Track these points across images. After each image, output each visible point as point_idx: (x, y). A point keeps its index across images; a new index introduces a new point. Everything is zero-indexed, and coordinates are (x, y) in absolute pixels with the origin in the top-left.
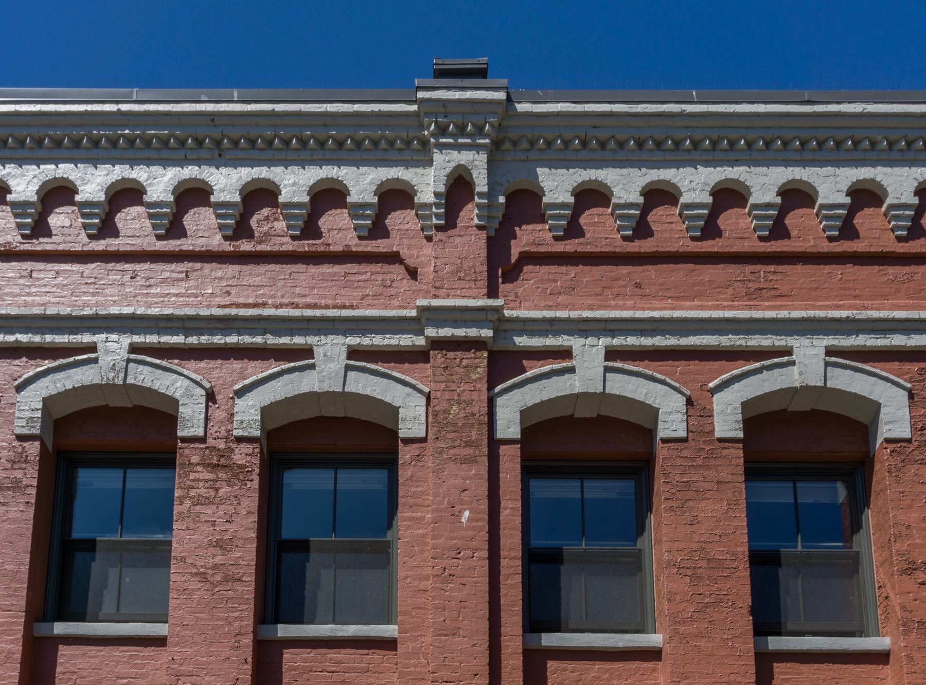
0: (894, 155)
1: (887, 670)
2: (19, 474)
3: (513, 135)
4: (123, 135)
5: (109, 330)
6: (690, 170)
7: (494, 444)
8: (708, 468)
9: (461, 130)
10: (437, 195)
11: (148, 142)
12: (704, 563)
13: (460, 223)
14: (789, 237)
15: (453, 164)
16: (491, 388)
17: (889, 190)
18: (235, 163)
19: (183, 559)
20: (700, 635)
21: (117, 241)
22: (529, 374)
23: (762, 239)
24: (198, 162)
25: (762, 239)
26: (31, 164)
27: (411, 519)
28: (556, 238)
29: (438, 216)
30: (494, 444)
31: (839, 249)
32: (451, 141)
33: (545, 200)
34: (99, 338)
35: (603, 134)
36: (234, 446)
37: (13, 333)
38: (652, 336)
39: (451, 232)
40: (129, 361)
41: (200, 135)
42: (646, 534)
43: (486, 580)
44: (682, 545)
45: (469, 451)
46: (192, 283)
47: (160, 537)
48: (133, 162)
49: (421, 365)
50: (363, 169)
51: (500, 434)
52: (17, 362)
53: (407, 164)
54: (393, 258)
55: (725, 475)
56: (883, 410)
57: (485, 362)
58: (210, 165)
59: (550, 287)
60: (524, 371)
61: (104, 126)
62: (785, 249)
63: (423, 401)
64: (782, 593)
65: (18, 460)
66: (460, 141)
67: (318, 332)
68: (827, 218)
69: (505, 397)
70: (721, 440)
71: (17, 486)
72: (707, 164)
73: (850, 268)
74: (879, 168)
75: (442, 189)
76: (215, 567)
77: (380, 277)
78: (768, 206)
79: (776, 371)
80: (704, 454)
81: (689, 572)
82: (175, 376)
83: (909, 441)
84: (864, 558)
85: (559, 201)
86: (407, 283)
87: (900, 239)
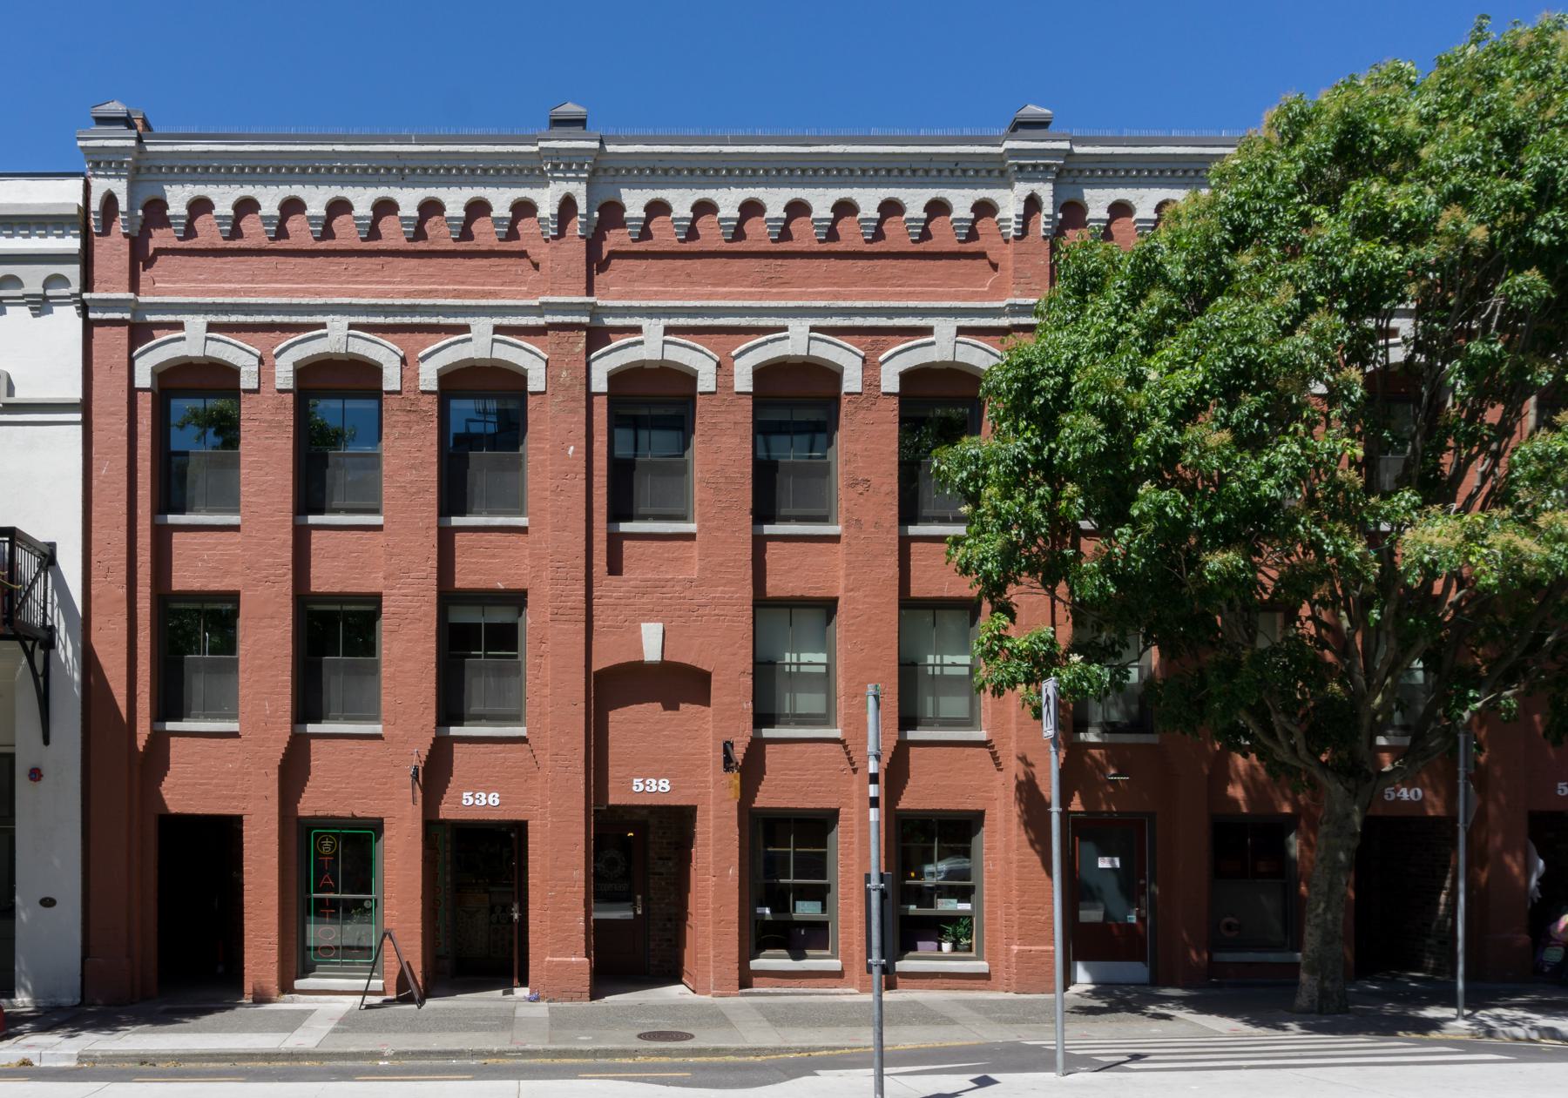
0: (866, 179)
2: (281, 418)
3: (605, 166)
4: (337, 167)
5: (334, 313)
6: (726, 190)
7: (590, 396)
8: (728, 412)
9: (568, 168)
10: (552, 215)
11: (353, 170)
12: (723, 480)
13: (568, 233)
14: (791, 239)
15: (563, 193)
16: (588, 353)
17: (861, 206)
18: (414, 185)
19: (391, 477)
20: (718, 529)
21: (334, 242)
22: (613, 345)
23: (773, 241)
24: (388, 184)
25: (773, 241)
26: (272, 185)
27: (537, 448)
28: (634, 241)
29: (553, 230)
30: (590, 396)
31: (825, 249)
32: (562, 175)
33: (626, 215)
34: (326, 319)
35: (667, 166)
36: (420, 397)
37: (270, 315)
38: (696, 318)
39: (562, 240)
40: (348, 336)
41: (389, 166)
42: (690, 449)
43: (584, 494)
44: (710, 467)
45: (573, 404)
46: (387, 273)
47: (368, 449)
48: (343, 184)
49: (542, 337)
50: (501, 189)
51: (594, 389)
52: (272, 335)
53: (532, 185)
54: (522, 254)
55: (739, 418)
56: (845, 372)
57: (584, 340)
58: (396, 186)
59: (629, 276)
61: (324, 160)
62: (788, 249)
63: (544, 365)
64: (778, 490)
65: (278, 408)
66: (568, 175)
67: (474, 315)
68: (817, 227)
69: (598, 361)
70: (738, 393)
71: (279, 424)
72: (737, 186)
73: (832, 262)
74: (855, 189)
75: (555, 211)
76: (411, 482)
77: (514, 269)
78: (777, 219)
79: (777, 343)
80: (726, 403)
81: (714, 486)
82: (379, 346)
83: (860, 394)
85: (635, 216)
86: (533, 275)
87: (867, 241)
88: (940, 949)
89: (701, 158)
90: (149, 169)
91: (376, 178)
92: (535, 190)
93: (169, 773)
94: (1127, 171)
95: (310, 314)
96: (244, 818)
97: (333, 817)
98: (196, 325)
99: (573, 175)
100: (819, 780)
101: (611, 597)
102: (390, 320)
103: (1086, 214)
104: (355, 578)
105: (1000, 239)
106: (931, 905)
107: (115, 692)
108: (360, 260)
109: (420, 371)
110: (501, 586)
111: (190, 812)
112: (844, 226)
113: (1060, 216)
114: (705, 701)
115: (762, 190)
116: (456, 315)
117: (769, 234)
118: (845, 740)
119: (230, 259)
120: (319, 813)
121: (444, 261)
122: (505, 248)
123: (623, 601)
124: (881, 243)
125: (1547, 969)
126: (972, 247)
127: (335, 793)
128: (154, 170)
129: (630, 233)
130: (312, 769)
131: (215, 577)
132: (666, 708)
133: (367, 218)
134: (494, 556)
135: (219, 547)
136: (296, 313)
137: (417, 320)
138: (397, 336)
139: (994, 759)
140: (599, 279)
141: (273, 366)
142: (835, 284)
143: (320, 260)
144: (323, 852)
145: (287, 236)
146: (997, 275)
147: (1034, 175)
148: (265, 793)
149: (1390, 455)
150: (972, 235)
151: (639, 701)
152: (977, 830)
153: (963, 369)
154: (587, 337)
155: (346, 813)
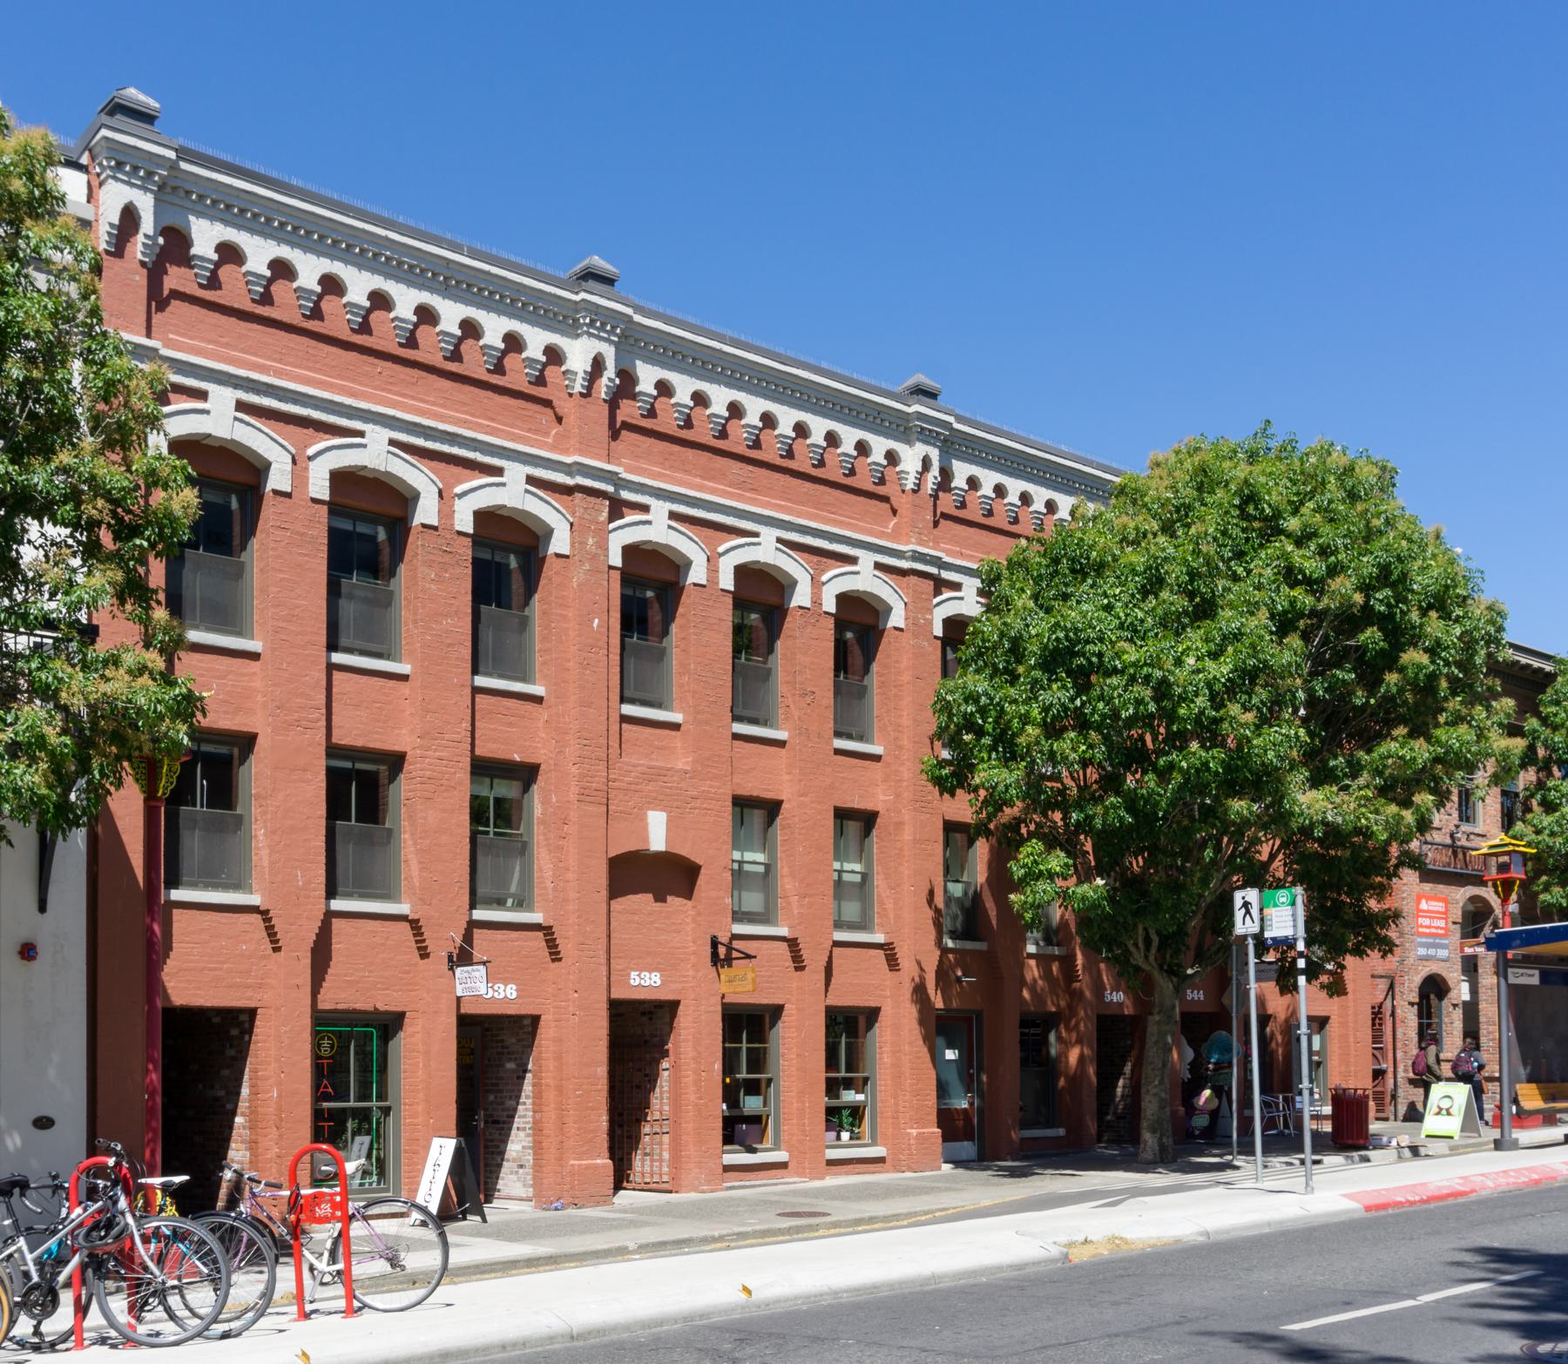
1: (783, 751)
5: (375, 422)
27: (561, 615)
28: (642, 416)
35: (676, 349)
52: (305, 431)
53: (563, 333)
54: (547, 403)
60: (622, 517)
67: (508, 458)
70: (722, 590)
84: (247, 568)
88: (838, 1138)
89: (705, 350)
90: (175, 189)
91: (420, 281)
92: (565, 339)
93: (172, 954)
94: (480, 290)
95: (350, 417)
96: (259, 1011)
97: (355, 1011)
98: (222, 399)
99: (605, 335)
100: (770, 976)
101: (622, 781)
102: (430, 445)
103: (951, 481)
104: (377, 733)
105: (898, 488)
106: (838, 1097)
107: (129, 848)
108: (394, 366)
109: (456, 508)
110: (517, 758)
111: (198, 1004)
112: (511, 361)
113: (161, 240)
114: (688, 893)
115: (744, 394)
116: (492, 454)
117: (746, 439)
118: (267, 912)
119: (255, 326)
120: (341, 1007)
121: (477, 391)
122: (534, 393)
123: (633, 787)
124: (541, 389)
125: (1197, 1133)
126: (881, 490)
127: (358, 982)
128: (182, 194)
129: (639, 408)
130: (334, 954)
131: (225, 712)
132: (657, 900)
133: (209, 261)
134: (510, 724)
135: (231, 677)
136: (333, 412)
137: (455, 451)
138: (434, 464)
139: (269, 935)
140: (157, 318)
141: (306, 469)
142: (789, 500)
143: (353, 355)
144: (323, 1053)
145: (322, 319)
146: (895, 520)
147: (929, 439)
148: (297, 981)
149: (201, 551)
150: (540, 381)
151: (635, 892)
152: (773, 1024)
153: (528, 523)
154: (610, 506)
155: (369, 1007)
